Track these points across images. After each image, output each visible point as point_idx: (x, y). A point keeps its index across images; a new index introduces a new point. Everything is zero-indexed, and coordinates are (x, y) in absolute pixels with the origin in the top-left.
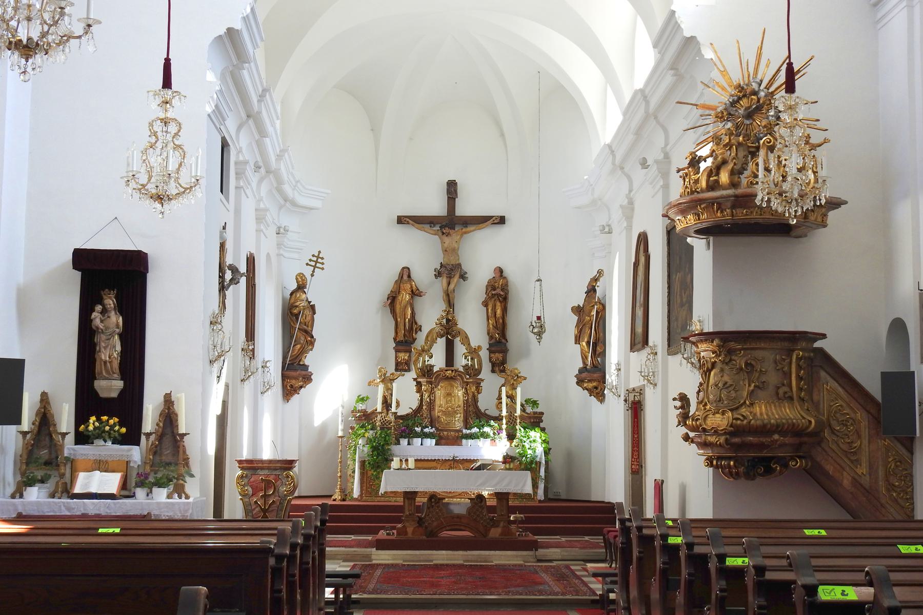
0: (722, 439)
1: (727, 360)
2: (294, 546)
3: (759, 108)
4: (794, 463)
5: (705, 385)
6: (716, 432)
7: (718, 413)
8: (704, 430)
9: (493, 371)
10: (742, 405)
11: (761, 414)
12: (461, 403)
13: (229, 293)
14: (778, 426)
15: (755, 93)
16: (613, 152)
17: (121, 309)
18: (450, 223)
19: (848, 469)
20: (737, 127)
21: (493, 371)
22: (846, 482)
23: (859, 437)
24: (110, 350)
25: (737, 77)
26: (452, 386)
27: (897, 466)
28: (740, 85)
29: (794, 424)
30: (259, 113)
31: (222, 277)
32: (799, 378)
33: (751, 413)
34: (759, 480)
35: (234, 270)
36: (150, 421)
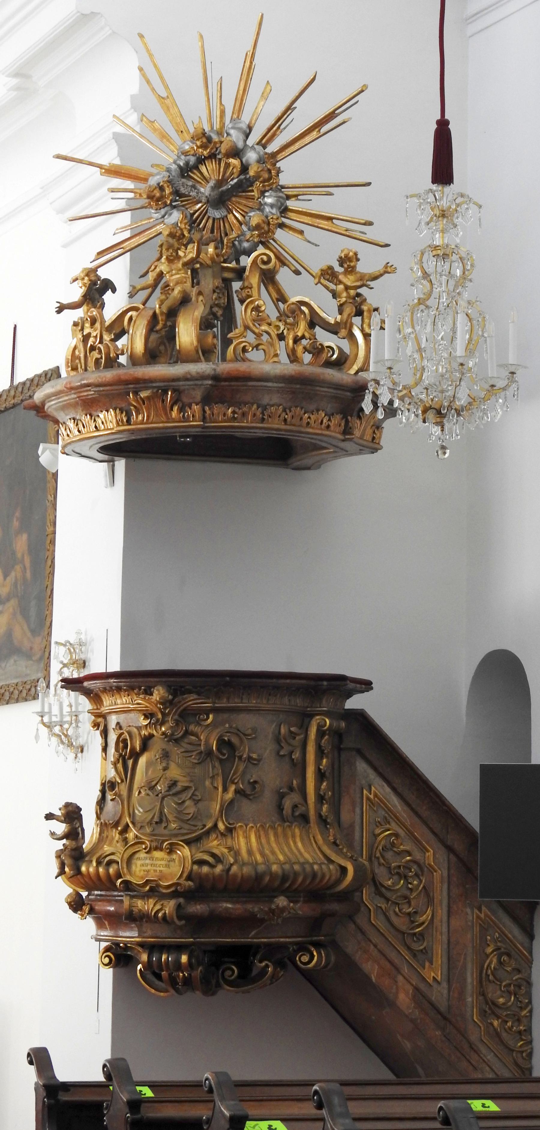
0: (169, 907)
1: (179, 734)
3: (244, 186)
4: (305, 958)
5: (123, 789)
6: (153, 890)
7: (159, 848)
8: (127, 886)
10: (208, 833)
11: (250, 852)
14: (284, 878)
15: (236, 153)
19: (405, 970)
20: (193, 222)
22: (404, 999)
23: (430, 901)
25: (197, 115)
27: (500, 963)
28: (204, 134)
29: (314, 875)
32: (321, 775)
33: (230, 849)
34: (226, 993)
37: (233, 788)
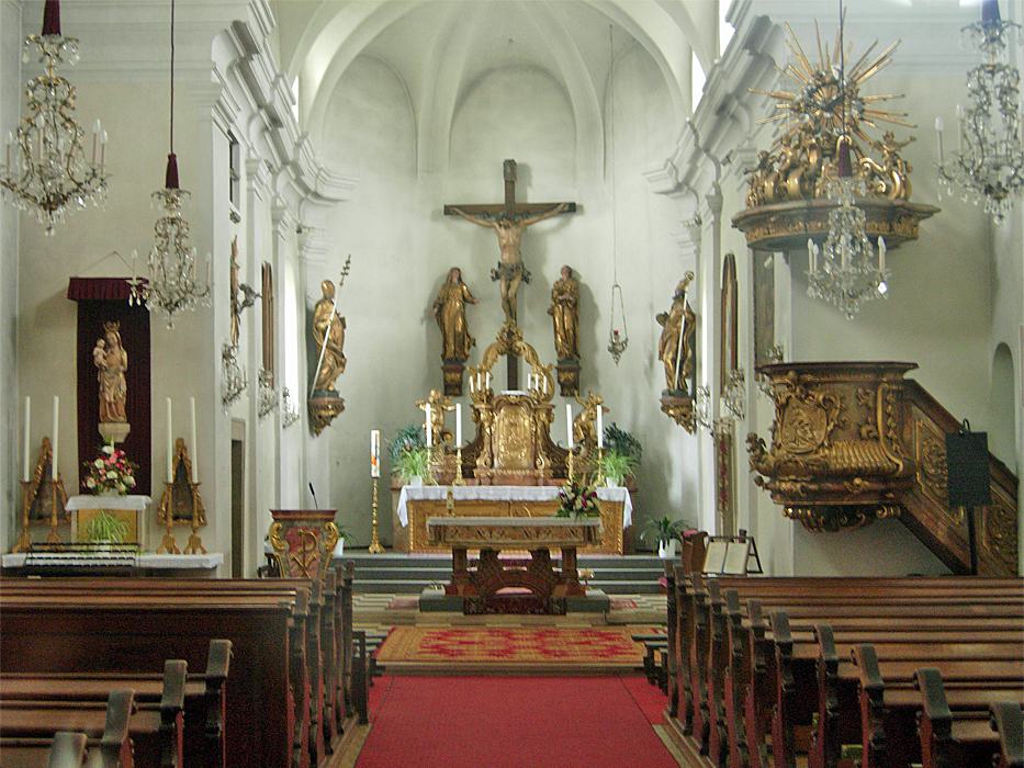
2: (313, 607)
9: (562, 395)
12: (528, 435)
13: (244, 315)
16: (695, 131)
17: (126, 343)
18: (514, 213)
21: (562, 395)
24: (114, 389)
26: (517, 414)
30: (272, 103)
31: (233, 297)
32: (887, 415)
35: (248, 290)
36: (163, 469)
37: (832, 424)
